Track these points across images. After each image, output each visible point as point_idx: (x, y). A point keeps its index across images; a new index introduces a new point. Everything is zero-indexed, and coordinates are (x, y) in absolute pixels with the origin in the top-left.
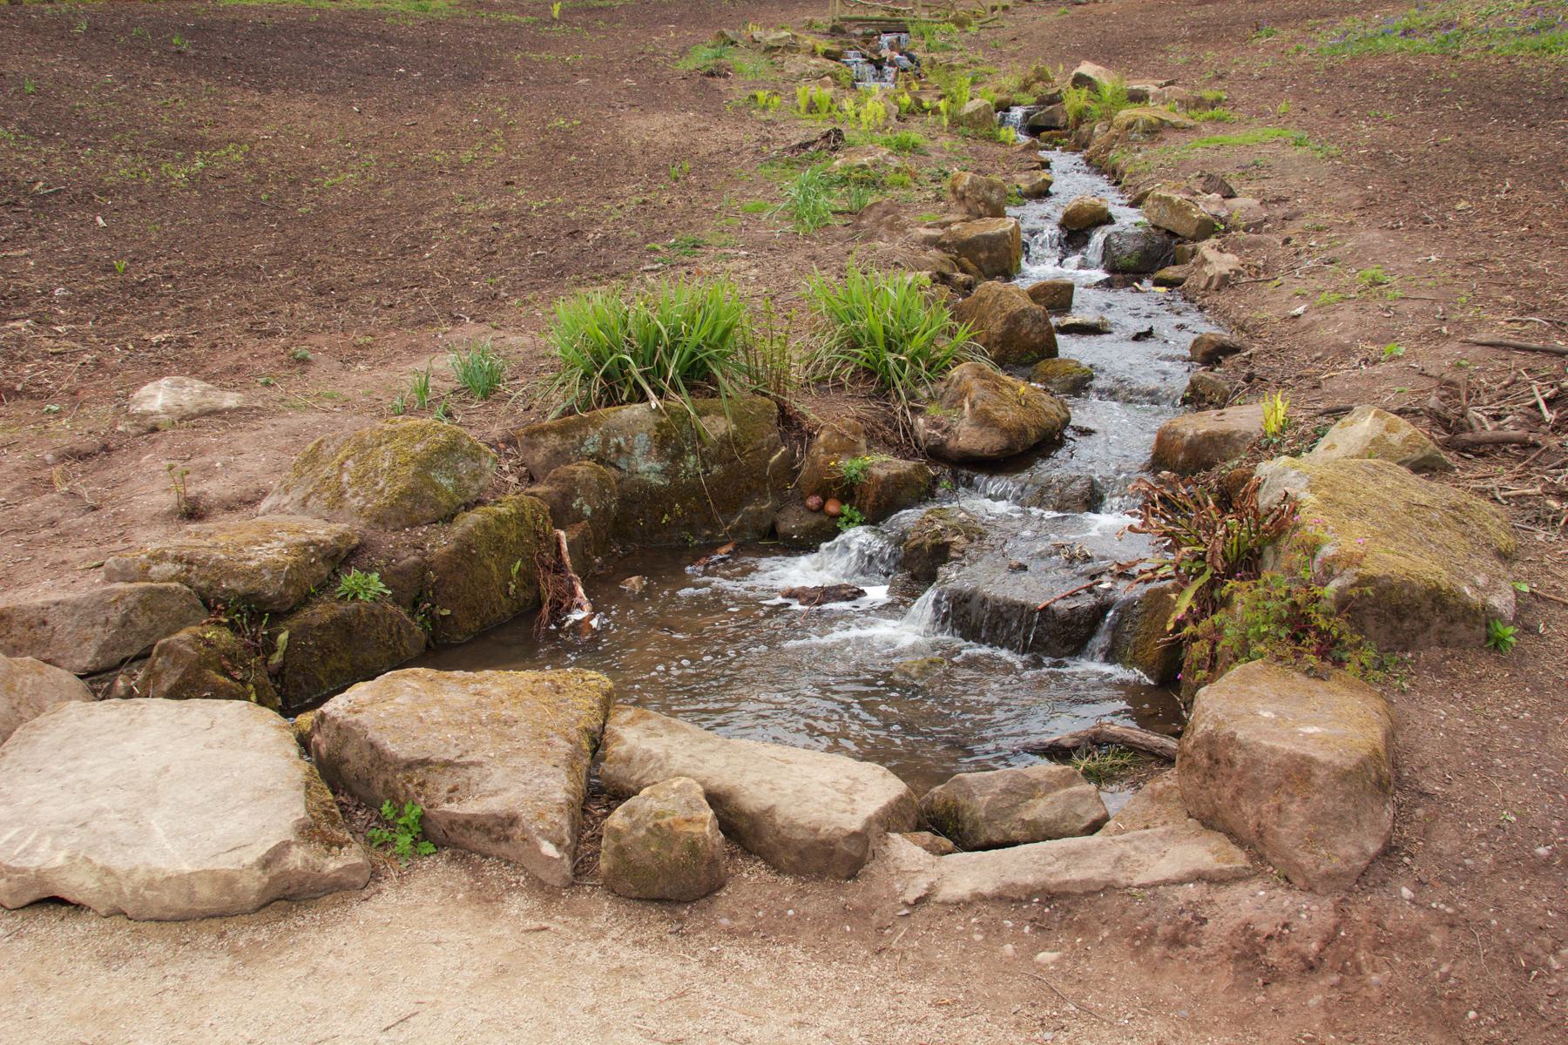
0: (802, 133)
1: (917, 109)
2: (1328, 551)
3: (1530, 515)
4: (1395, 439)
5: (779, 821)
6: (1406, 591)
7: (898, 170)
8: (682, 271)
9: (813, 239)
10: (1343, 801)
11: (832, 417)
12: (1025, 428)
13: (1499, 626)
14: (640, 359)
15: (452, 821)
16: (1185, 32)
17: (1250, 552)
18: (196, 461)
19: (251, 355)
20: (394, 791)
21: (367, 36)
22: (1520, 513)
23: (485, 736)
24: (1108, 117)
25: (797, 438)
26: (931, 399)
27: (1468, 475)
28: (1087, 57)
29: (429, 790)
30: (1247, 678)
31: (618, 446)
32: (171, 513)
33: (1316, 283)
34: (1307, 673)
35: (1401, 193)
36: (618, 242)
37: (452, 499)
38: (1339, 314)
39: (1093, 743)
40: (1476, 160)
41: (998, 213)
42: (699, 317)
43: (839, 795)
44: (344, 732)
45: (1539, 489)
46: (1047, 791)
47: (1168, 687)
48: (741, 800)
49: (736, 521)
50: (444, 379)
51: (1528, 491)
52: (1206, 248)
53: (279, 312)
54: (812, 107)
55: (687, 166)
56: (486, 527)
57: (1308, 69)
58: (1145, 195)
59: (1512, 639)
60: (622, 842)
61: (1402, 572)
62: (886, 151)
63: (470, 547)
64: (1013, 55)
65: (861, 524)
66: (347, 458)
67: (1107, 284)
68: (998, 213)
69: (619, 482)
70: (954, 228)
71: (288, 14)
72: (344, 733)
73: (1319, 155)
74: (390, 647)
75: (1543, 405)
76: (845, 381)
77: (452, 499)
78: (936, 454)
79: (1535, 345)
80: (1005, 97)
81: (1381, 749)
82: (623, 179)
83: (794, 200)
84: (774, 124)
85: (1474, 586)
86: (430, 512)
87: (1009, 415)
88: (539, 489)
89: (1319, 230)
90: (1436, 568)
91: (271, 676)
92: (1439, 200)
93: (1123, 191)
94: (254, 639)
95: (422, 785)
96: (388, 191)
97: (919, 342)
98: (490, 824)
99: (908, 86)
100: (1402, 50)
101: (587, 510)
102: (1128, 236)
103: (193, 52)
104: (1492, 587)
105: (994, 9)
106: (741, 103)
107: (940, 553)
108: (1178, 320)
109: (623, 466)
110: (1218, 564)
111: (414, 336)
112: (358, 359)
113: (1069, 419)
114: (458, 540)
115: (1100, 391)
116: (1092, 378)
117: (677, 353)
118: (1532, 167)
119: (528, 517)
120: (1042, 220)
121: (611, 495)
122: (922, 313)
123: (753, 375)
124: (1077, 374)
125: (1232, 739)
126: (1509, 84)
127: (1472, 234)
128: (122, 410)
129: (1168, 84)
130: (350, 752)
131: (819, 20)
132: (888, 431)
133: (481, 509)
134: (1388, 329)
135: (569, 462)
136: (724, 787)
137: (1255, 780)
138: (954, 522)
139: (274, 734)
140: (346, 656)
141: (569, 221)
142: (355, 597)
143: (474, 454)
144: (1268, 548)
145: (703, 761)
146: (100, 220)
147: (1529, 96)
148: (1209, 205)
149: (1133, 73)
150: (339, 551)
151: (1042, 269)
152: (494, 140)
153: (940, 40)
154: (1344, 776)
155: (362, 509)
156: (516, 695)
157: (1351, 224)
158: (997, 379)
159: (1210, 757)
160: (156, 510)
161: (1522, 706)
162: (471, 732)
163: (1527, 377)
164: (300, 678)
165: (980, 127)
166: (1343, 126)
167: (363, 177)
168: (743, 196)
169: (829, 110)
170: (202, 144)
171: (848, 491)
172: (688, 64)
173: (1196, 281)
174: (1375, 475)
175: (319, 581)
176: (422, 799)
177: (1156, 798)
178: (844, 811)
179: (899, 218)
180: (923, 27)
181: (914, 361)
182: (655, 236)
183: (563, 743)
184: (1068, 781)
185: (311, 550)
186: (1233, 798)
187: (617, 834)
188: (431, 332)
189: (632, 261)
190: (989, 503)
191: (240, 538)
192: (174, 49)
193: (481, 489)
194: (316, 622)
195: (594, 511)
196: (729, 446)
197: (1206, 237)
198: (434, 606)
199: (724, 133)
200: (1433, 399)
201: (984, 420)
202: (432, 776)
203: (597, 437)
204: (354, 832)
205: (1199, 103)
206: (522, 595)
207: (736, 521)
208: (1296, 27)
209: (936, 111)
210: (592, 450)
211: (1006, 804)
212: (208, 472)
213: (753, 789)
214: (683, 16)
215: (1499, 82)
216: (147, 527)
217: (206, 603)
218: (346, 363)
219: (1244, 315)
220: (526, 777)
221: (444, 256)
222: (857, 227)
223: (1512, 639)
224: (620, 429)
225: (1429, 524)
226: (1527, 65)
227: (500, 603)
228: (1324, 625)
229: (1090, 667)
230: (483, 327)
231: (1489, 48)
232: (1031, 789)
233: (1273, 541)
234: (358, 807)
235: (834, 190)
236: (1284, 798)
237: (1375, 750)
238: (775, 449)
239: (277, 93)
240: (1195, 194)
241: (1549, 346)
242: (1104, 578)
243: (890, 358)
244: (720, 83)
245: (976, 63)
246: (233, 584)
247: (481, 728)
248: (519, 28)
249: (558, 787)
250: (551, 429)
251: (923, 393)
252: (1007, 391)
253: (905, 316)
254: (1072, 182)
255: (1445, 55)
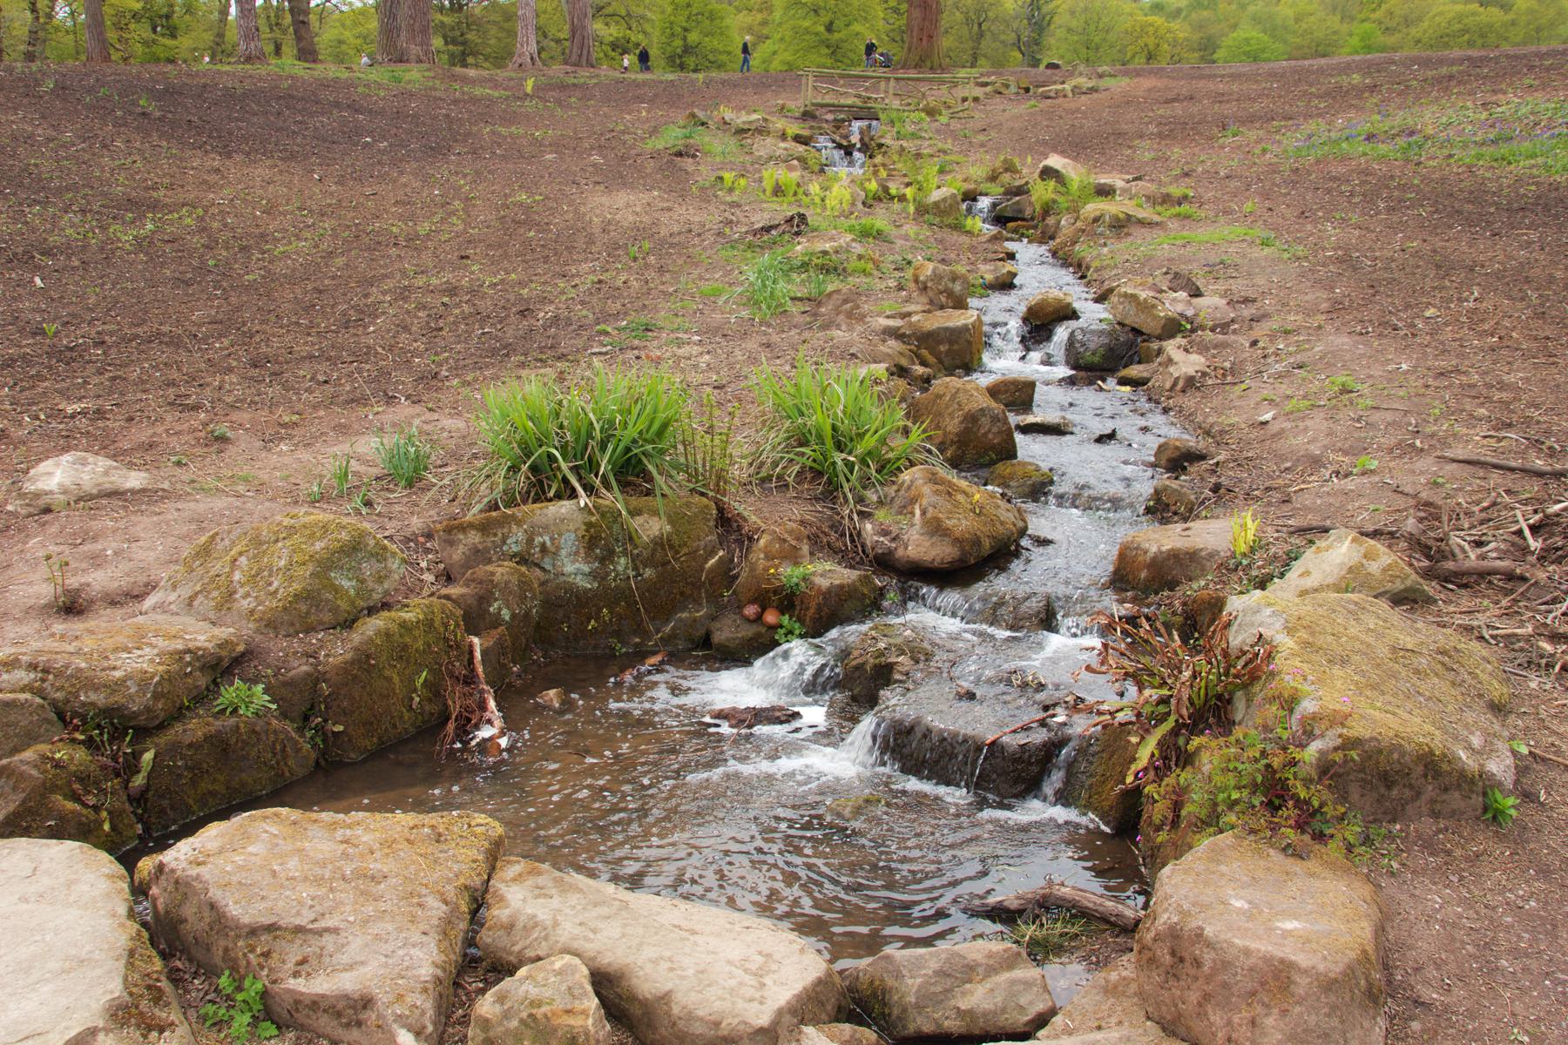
0: (766, 216)
1: (884, 196)
2: (1308, 706)
3: (1522, 658)
4: (1374, 567)
5: (676, 1010)
6: (1396, 756)
7: (860, 257)
8: (630, 355)
9: (769, 326)
10: (1328, 1015)
11: (774, 519)
12: (978, 538)
13: (1499, 796)
14: (571, 454)
15: (298, 1001)
16: (1152, 128)
17: (1219, 697)
18: (87, 547)
19: (167, 431)
20: (235, 960)
21: (337, 105)
22: (1511, 655)
23: (346, 895)
24: (1075, 210)
25: (736, 541)
26: (881, 503)
27: (1452, 608)
28: (1055, 150)
29: (274, 961)
30: (1216, 856)
31: (543, 545)
32: (48, 606)
33: (1285, 388)
34: (1284, 850)
35: (1370, 297)
36: (569, 322)
37: (352, 603)
38: (1309, 423)
39: (1041, 906)
40: (1443, 267)
41: (960, 304)
42: (635, 411)
43: (747, 978)
44: (183, 887)
45: (1529, 629)
46: (987, 976)
47: (1128, 840)
48: (634, 981)
49: (668, 629)
50: (367, 463)
51: (1518, 631)
52: (1172, 347)
53: (208, 385)
54: (778, 191)
55: (647, 245)
56: (388, 635)
57: (1274, 169)
58: (1111, 290)
59: (1513, 812)
60: (491, 1034)
61: (1391, 734)
62: (849, 237)
63: (368, 657)
64: (982, 145)
65: (801, 636)
66: (241, 554)
67: (1071, 382)
68: (960, 304)
69: (542, 584)
70: (915, 318)
71: (260, 80)
72: (182, 889)
73: (1286, 256)
74: (272, 767)
75: (1527, 532)
76: (790, 480)
77: (352, 603)
78: (884, 563)
79: (1513, 464)
80: (972, 186)
81: (1370, 948)
82: (581, 257)
83: (752, 284)
84: (738, 206)
85: (1469, 748)
86: (327, 617)
87: (962, 524)
88: (455, 590)
89: (1287, 332)
90: (1428, 727)
91: (130, 799)
92: (1407, 307)
93: (1088, 285)
94: (115, 758)
95: (267, 955)
96: (340, 261)
97: (870, 442)
98: (340, 1006)
99: (875, 173)
100: (1365, 154)
101: (506, 614)
102: (1092, 332)
103: (158, 114)
104: (1488, 750)
105: (964, 100)
106: (707, 184)
107: (883, 675)
108: (1142, 422)
109: (548, 567)
110: (1185, 712)
111: (343, 415)
112: (282, 439)
113: (1026, 528)
114: (356, 649)
115: (1060, 497)
116: (1052, 482)
117: (610, 447)
118: (1498, 276)
119: (437, 623)
120: (1003, 314)
121: (532, 599)
122: (874, 410)
123: (693, 476)
124: (1036, 478)
125: (1199, 935)
126: (1471, 193)
127: (1442, 343)
128: (16, 487)
129: (1135, 179)
130: (188, 911)
131: (791, 105)
132: (834, 536)
133: (385, 614)
134: (1359, 440)
135: (490, 562)
136: (615, 967)
137: (1225, 985)
138: (899, 641)
139: (104, 885)
140: (221, 778)
141: (520, 298)
142: (235, 711)
143: (380, 554)
144: (1239, 694)
145: (594, 931)
146: (38, 281)
147: (1491, 205)
148: (1175, 304)
149: (1102, 167)
150: (220, 659)
151: (1005, 362)
152: (453, 213)
153: (910, 128)
154: (1329, 985)
155: (252, 612)
156: (388, 844)
157: (1320, 327)
158: (950, 484)
159: (1173, 953)
160: (32, 602)
161: (1526, 892)
162: (332, 890)
163: (1507, 499)
164: (165, 803)
165: (945, 216)
166: (1309, 227)
167: (316, 246)
168: (701, 278)
169: (795, 194)
170: (155, 206)
171: (788, 600)
172: (659, 143)
173: (1161, 381)
174: (1356, 612)
175: (195, 693)
176: (265, 972)
177: (1110, 990)
178: (751, 1000)
179: (858, 307)
180: (894, 115)
181: (863, 462)
182: (605, 317)
183: (438, 904)
184: (1009, 963)
185: (188, 658)
186: (1200, 1004)
187: (485, 1024)
188: (362, 411)
189: (579, 343)
190: (936, 619)
191: (109, 643)
192: (139, 110)
193: (387, 593)
194: (187, 739)
195: (513, 616)
196: (663, 548)
197: (1172, 336)
198: (326, 721)
199: (688, 213)
200: (1411, 521)
201: (935, 528)
202: (280, 945)
203: (521, 536)
204: (185, 1007)
205: (1166, 199)
206: (427, 708)
207: (668, 629)
208: (1261, 128)
209: (902, 198)
210: (515, 549)
211: (939, 989)
212: (97, 561)
213: (649, 968)
214: (656, 96)
215: (1460, 190)
216: (19, 621)
217: (61, 716)
218: (268, 442)
219: (1211, 420)
220: (389, 948)
221: (388, 331)
222: (815, 315)
223: (1513, 812)
224: (546, 528)
225: (1417, 672)
226: (1488, 175)
227: (401, 717)
228: (1303, 795)
229: (1035, 811)
230: (418, 409)
231: (1451, 156)
232: (969, 972)
233: (1245, 686)
234: (196, 975)
235: (794, 276)
236: (1259, 1009)
237: (1364, 952)
238: (712, 553)
239: (238, 158)
240: (1161, 291)
241: (1528, 466)
242: (1059, 710)
243: (838, 458)
244: (688, 164)
245: (945, 152)
246: (93, 697)
247: (343, 885)
248: (492, 102)
249: (425, 959)
250: (471, 525)
251: (871, 496)
252: (960, 498)
253: (855, 414)
254: (1038, 275)
255: (1407, 161)
